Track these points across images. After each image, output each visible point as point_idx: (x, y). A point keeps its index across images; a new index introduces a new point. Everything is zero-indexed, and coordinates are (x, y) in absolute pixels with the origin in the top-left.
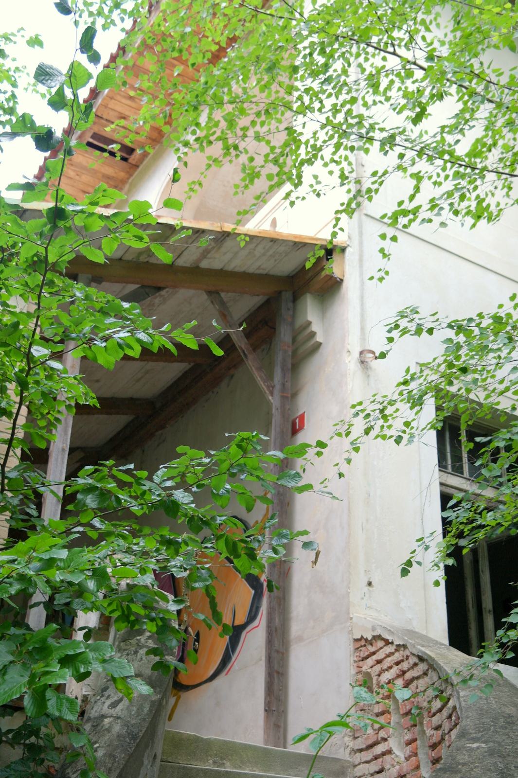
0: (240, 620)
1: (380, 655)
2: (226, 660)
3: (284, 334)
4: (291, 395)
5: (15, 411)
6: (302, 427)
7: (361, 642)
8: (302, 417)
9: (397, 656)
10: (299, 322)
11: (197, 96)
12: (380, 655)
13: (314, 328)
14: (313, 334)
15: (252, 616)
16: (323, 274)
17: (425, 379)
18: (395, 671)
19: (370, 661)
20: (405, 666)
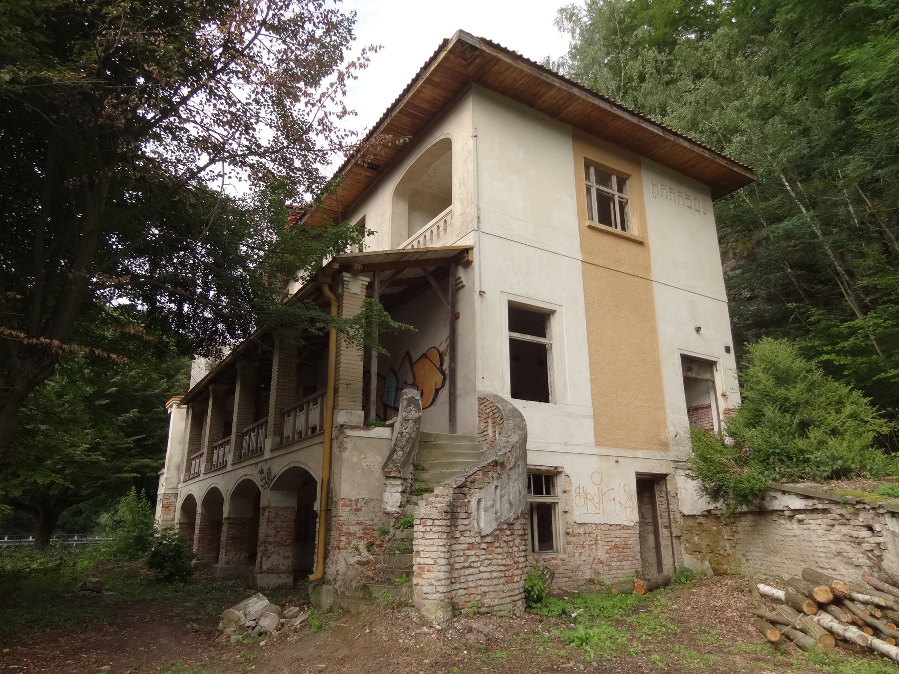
0: (439, 386)
1: (486, 404)
2: (434, 401)
3: (452, 282)
4: (454, 304)
5: (674, 541)
6: (459, 318)
7: (480, 399)
8: (459, 313)
9: (491, 405)
10: (457, 277)
11: (487, 650)
12: (486, 404)
13: (462, 279)
14: (462, 282)
15: (443, 385)
16: (464, 260)
17: (757, 85)
18: (490, 409)
19: (483, 405)
20: (493, 408)
